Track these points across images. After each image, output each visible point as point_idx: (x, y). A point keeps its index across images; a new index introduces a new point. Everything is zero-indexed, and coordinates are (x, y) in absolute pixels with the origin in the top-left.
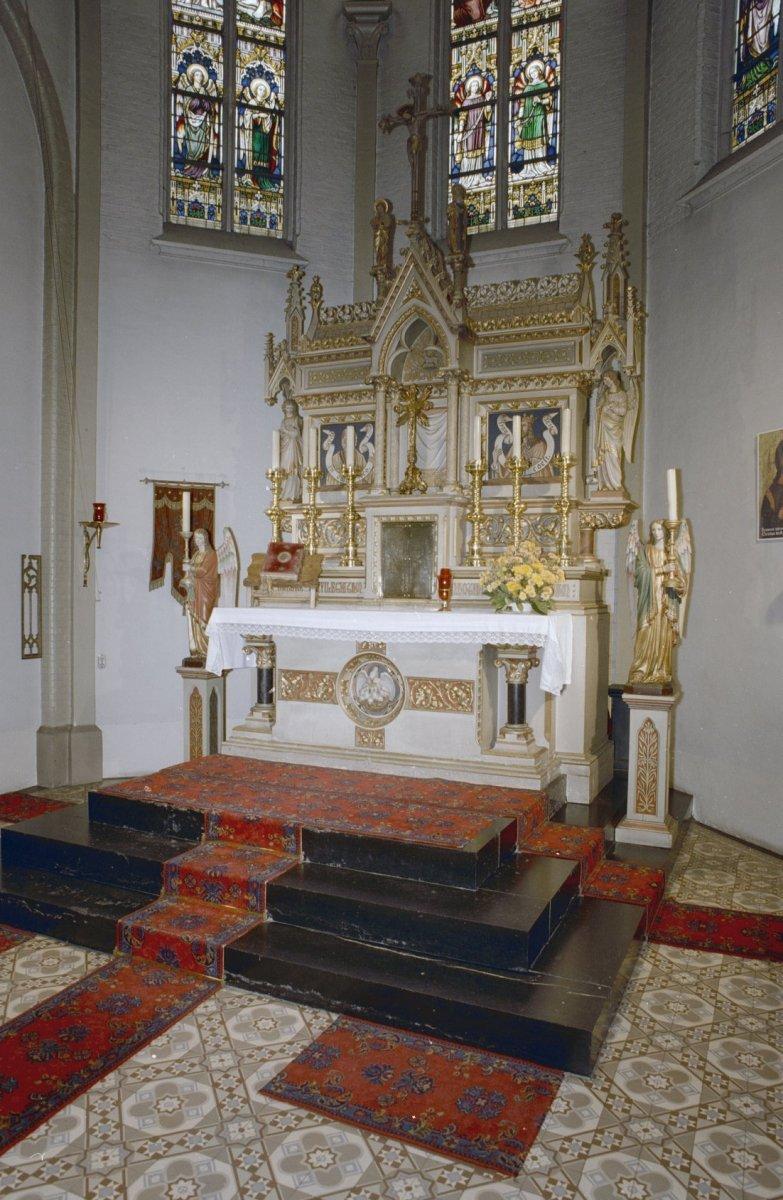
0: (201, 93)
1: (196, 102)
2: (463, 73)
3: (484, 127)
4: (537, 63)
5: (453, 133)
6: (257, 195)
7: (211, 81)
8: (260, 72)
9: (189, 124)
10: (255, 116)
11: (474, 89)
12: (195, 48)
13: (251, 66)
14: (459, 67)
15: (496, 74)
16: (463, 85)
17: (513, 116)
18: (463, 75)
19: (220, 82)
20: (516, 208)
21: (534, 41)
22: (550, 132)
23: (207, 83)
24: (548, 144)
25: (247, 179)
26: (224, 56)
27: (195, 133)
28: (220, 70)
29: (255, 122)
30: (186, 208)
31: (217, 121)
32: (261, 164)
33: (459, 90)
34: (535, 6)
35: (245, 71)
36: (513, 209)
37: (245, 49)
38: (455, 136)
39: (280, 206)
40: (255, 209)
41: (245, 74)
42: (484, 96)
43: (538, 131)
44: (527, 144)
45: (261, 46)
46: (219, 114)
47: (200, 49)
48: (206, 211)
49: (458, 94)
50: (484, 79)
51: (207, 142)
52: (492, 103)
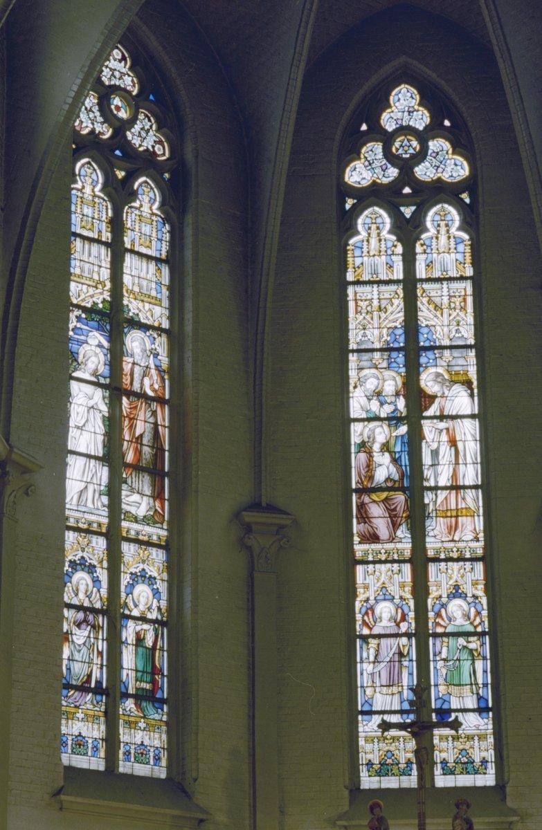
0: (85, 605)
1: (81, 615)
2: (371, 594)
3: (400, 661)
4: (458, 601)
5: (362, 662)
6: (140, 724)
7: (95, 590)
8: (142, 577)
9: (73, 641)
10: (138, 628)
11: (386, 616)
12: (80, 554)
13: (133, 570)
14: (366, 587)
15: (412, 603)
16: (372, 609)
17: (435, 655)
18: (372, 598)
19: (104, 592)
20: (444, 762)
21: (455, 577)
22: (480, 681)
23: (92, 592)
24: (478, 694)
25: (130, 704)
26: (108, 561)
27: (79, 651)
28: (103, 575)
29: (138, 634)
30: (70, 743)
31: (100, 637)
32: (144, 685)
33: (366, 613)
34: (453, 541)
35: (128, 576)
36: (441, 762)
37: (128, 549)
38: (365, 665)
39: (164, 737)
40: (139, 743)
41: (128, 580)
42: (398, 625)
43: (466, 678)
44: (454, 690)
45: (143, 547)
46: (103, 628)
47: (85, 555)
48: (90, 746)
49: (366, 618)
50: (397, 607)
51: (90, 662)
52: (408, 635)
